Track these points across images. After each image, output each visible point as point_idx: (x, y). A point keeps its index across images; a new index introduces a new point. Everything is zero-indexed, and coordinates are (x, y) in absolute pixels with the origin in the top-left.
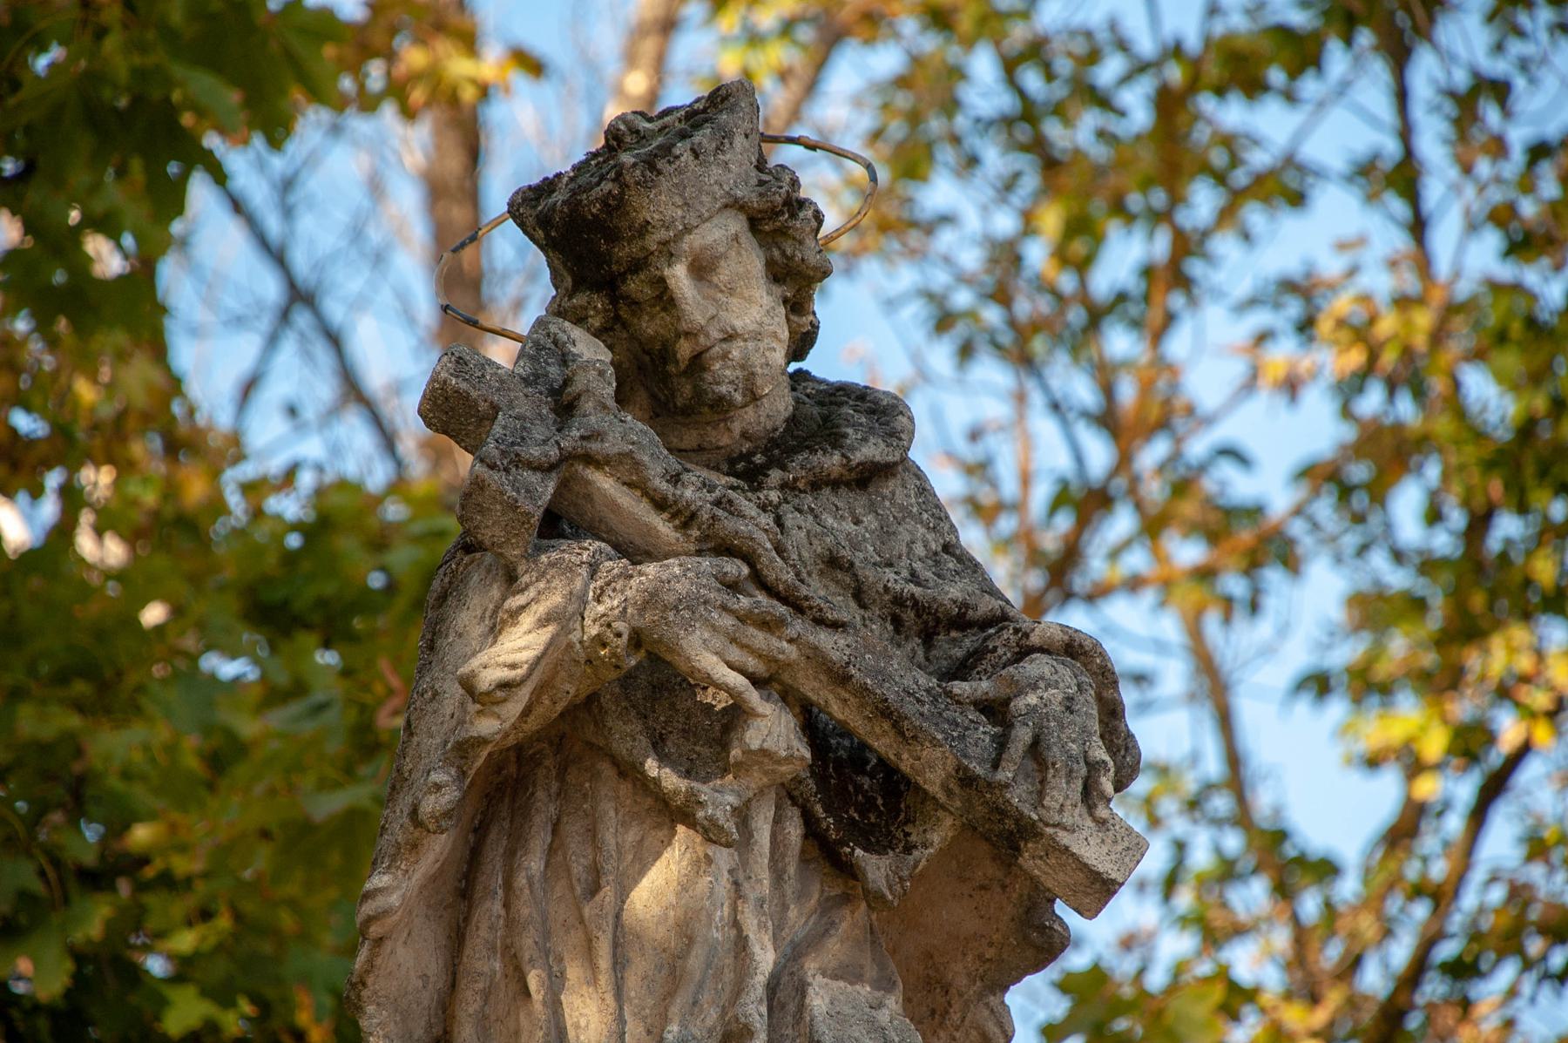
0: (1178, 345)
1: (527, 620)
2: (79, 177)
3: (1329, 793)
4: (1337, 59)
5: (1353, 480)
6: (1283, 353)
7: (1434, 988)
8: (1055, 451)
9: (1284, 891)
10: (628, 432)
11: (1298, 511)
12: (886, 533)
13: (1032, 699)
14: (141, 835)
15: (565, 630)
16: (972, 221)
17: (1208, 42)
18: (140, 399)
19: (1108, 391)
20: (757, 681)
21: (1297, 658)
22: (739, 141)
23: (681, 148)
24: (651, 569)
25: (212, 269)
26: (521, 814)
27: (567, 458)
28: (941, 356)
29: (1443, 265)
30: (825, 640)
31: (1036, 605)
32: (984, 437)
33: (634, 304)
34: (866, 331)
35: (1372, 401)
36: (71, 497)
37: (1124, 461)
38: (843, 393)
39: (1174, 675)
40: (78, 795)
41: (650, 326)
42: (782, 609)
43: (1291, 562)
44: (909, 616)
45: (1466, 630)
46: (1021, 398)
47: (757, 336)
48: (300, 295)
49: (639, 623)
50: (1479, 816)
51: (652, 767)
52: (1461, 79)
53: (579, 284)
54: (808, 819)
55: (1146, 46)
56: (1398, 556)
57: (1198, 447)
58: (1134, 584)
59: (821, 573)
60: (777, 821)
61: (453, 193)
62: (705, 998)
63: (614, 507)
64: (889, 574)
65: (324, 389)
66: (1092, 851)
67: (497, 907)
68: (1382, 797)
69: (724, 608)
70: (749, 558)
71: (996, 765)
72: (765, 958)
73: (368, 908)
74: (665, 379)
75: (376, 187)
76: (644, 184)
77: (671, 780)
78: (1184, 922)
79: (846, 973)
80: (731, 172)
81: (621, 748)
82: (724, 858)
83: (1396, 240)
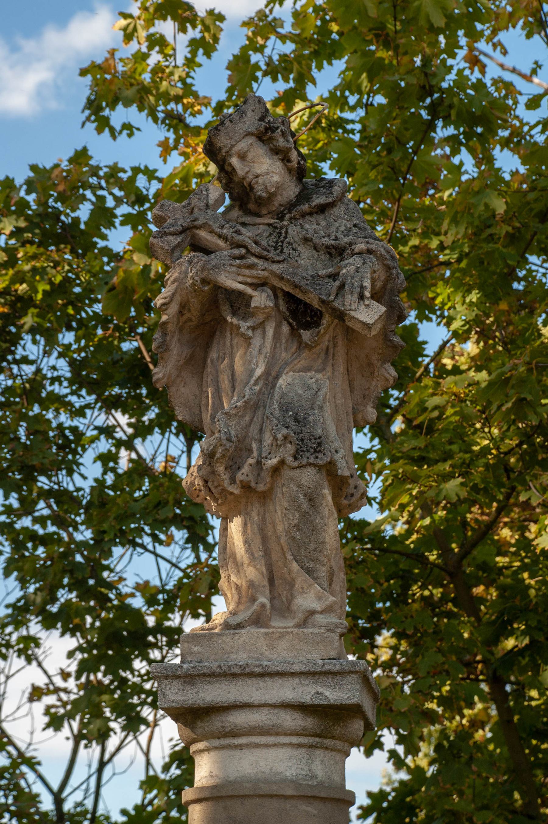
20: (250, 285)
44: (333, 251)
47: (267, 174)
49: (202, 276)
54: (290, 324)
59: (304, 244)
69: (231, 265)
70: (245, 247)
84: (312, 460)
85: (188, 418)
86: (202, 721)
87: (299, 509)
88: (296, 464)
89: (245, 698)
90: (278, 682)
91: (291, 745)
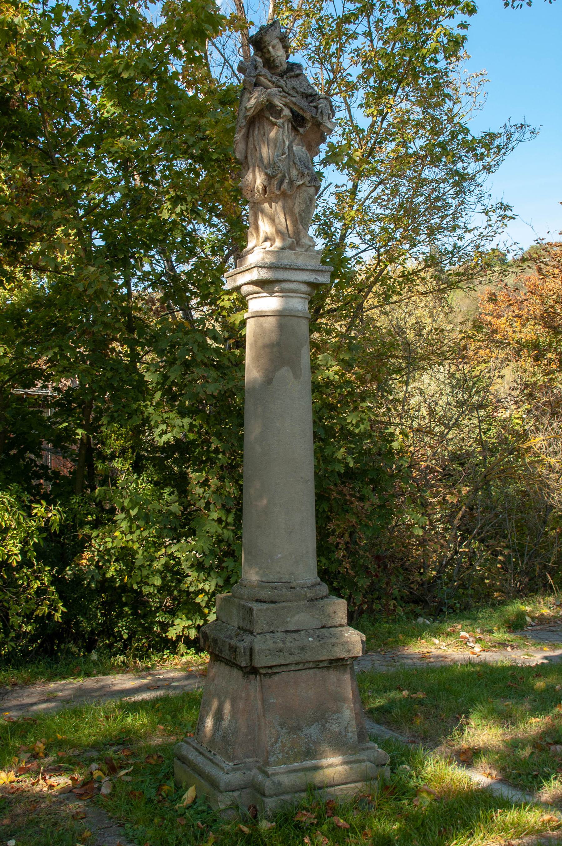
0: (341, 60)
2: (192, 41)
3: (363, 121)
4: (360, 18)
5: (363, 78)
7: (377, 146)
8: (325, 76)
9: (357, 134)
10: (265, 71)
19: (332, 67)
21: (359, 102)
26: (254, 125)
28: (310, 63)
30: (293, 99)
34: (297, 58)
41: (267, 56)
48: (226, 61)
50: (382, 122)
56: (370, 87)
57: (344, 74)
58: (337, 94)
66: (329, 125)
68: (370, 120)
74: (269, 64)
77: (273, 120)
80: (276, 33)
83: (368, 43)
90: (302, 273)
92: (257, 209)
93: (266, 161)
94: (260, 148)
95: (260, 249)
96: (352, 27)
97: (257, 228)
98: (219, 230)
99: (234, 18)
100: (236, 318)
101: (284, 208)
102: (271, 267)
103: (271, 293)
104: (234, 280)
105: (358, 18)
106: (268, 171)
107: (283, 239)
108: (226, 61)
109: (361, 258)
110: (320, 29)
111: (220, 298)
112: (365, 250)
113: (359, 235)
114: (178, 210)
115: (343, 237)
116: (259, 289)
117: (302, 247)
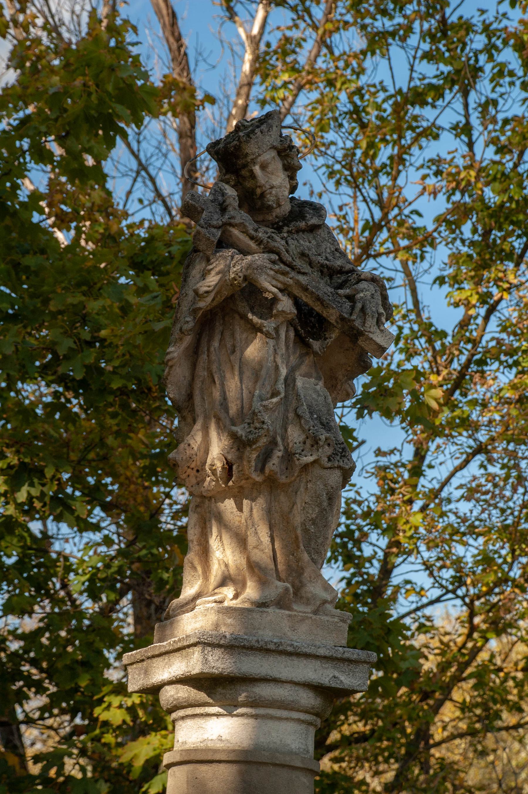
0: (401, 181)
1: (213, 273)
3: (442, 311)
4: (448, 96)
5: (451, 221)
6: (431, 181)
7: (474, 367)
8: (363, 213)
9: (430, 341)
10: (242, 216)
11: (435, 230)
12: (318, 246)
13: (362, 295)
14: (103, 333)
15: (224, 276)
16: (340, 144)
17: (409, 89)
18: (98, 201)
19: (380, 195)
20: (281, 290)
21: (435, 273)
22: (274, 128)
23: (257, 131)
24: (249, 257)
25: (118, 161)
27: (225, 224)
28: (331, 185)
29: (478, 158)
30: (301, 278)
31: (359, 260)
32: (344, 209)
33: (244, 178)
35: (457, 197)
36: (78, 229)
37: (385, 216)
38: (306, 203)
39: (400, 278)
40: (84, 319)
41: (248, 184)
42: (288, 269)
43: (433, 245)
44: (325, 270)
45: (485, 265)
46: (355, 197)
47: (280, 187)
48: (142, 167)
50: (487, 319)
51: (250, 316)
52: (483, 100)
53: (227, 172)
54: (296, 331)
55: (392, 91)
56: (463, 241)
58: (387, 253)
60: (287, 331)
61: (187, 136)
62: (266, 383)
63: (239, 239)
64: (319, 258)
65: (151, 195)
66: (379, 339)
67: (205, 357)
68: (460, 313)
70: (278, 254)
71: (351, 314)
72: (284, 372)
73: (168, 357)
74: (253, 201)
75: (164, 134)
76: (247, 142)
77: (255, 319)
78: (401, 351)
79: (307, 375)
81: (241, 310)
82: (272, 342)
83: (465, 149)
84: (341, 464)
85: (177, 397)
86: (224, 688)
87: (320, 505)
88: (329, 465)
89: (275, 673)
91: (299, 721)
92: (204, 508)
93: (233, 409)
94: (223, 379)
95: (208, 603)
96: (428, 114)
97: (205, 553)
98: (107, 541)
99: (170, 85)
100: (141, 750)
101: (269, 512)
102: (232, 647)
103: (230, 707)
104: (147, 672)
105: (442, 96)
106: (239, 430)
107: (263, 583)
108: (142, 167)
109: (429, 619)
110: (356, 113)
111: (101, 701)
112: (438, 600)
113: (428, 567)
114: (22, 496)
115: (387, 571)
116: (202, 696)
117: (308, 602)
